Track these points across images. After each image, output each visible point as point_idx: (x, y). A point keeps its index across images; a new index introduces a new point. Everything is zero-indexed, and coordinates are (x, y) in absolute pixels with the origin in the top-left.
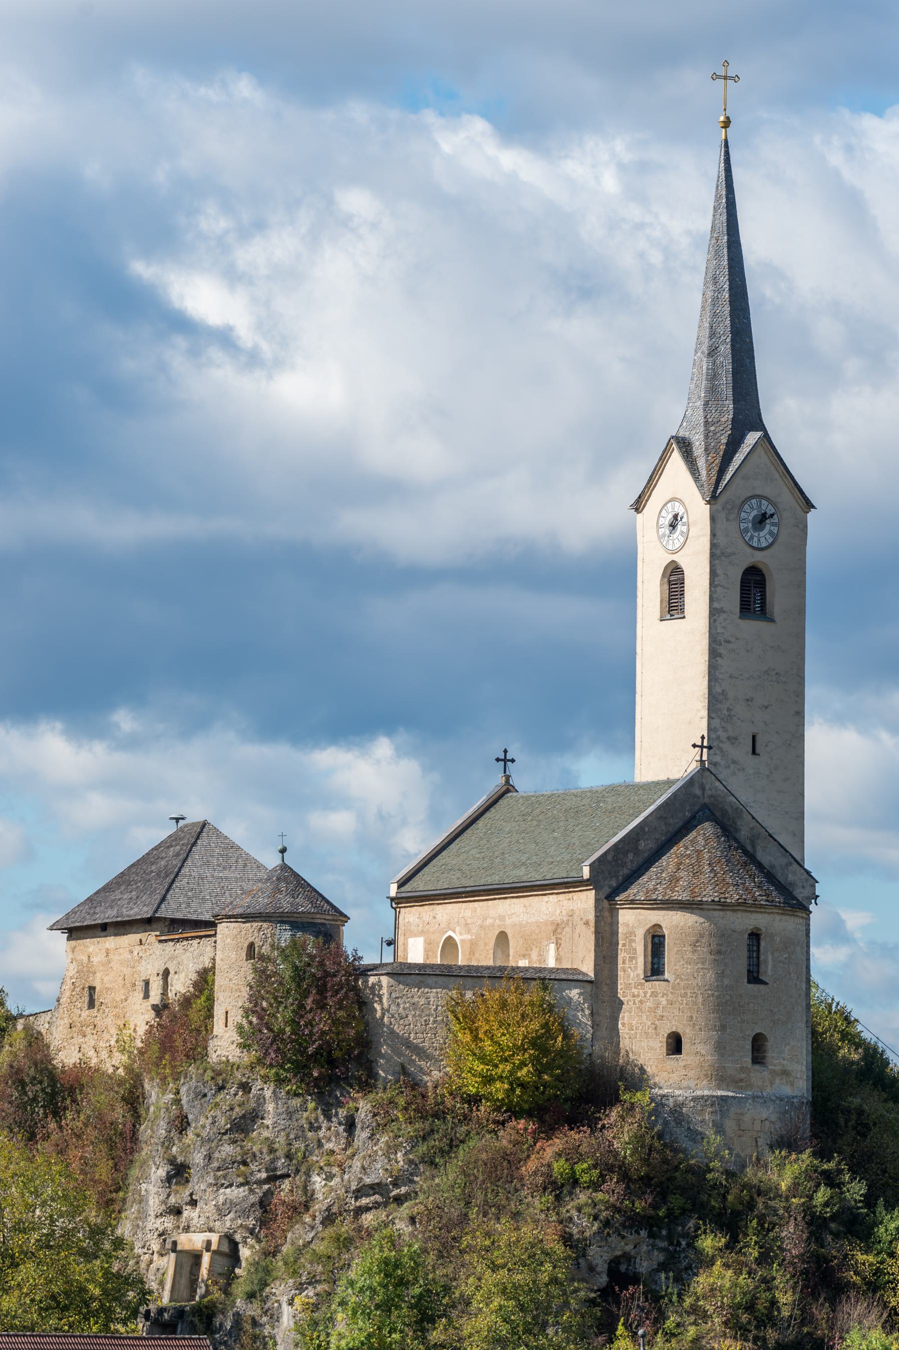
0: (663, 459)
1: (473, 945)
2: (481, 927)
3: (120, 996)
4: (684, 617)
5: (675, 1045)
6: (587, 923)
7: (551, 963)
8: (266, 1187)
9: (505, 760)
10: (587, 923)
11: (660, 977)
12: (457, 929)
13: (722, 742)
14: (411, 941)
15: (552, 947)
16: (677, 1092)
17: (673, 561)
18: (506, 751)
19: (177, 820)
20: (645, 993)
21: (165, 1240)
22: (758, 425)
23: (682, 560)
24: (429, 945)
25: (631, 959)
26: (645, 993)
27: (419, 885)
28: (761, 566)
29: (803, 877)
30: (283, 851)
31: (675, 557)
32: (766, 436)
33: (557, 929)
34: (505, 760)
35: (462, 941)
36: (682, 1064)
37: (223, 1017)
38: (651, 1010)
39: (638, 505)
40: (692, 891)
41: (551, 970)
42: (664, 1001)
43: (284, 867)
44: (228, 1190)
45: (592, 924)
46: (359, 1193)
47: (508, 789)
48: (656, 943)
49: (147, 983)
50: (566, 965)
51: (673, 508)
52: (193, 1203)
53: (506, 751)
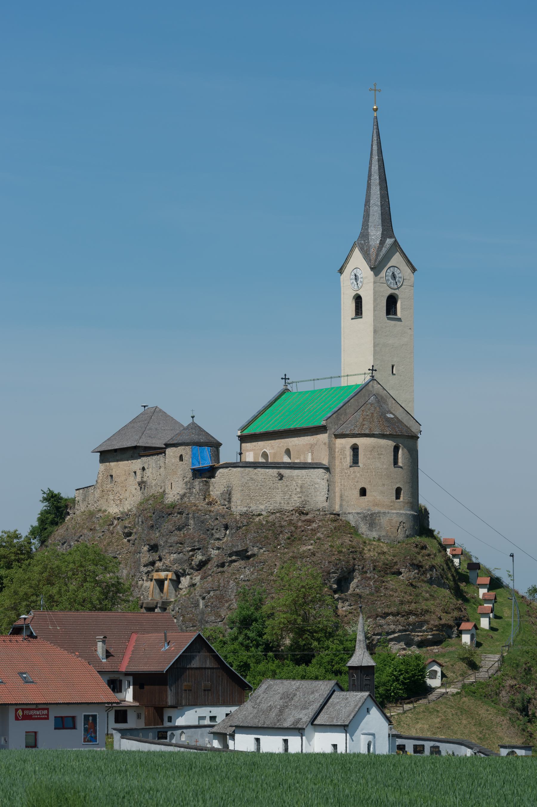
0: (352, 251)
1: (275, 454)
2: (278, 447)
3: (123, 479)
4: (361, 318)
5: (363, 492)
6: (325, 444)
7: (310, 461)
8: (191, 553)
9: (285, 379)
10: (325, 444)
11: (357, 465)
12: (268, 448)
13: (108, 706)
14: (247, 453)
15: (310, 454)
16: (364, 512)
17: (357, 294)
18: (285, 375)
19: (145, 406)
20: (351, 472)
21: (148, 575)
22: (392, 236)
23: (361, 293)
24: (255, 455)
25: (344, 458)
26: (351, 472)
27: (253, 429)
28: (394, 295)
29: (335, 721)
30: (193, 417)
31: (358, 292)
32: (396, 241)
33: (312, 447)
34: (285, 379)
35: (270, 453)
36: (366, 500)
37: (170, 485)
38: (353, 479)
39: (341, 271)
40: (370, 429)
41: (310, 463)
42: (358, 475)
43: (193, 423)
44: (175, 555)
45: (327, 444)
46: (230, 555)
47: (286, 391)
48: (355, 449)
49: (135, 472)
50: (315, 461)
51: (391, 271)
52: (160, 560)
53: (285, 375)
